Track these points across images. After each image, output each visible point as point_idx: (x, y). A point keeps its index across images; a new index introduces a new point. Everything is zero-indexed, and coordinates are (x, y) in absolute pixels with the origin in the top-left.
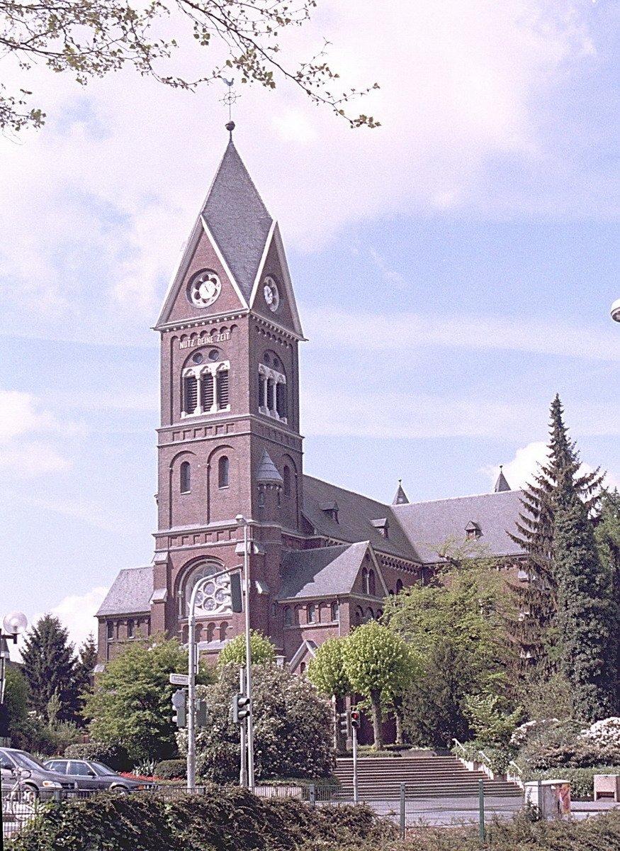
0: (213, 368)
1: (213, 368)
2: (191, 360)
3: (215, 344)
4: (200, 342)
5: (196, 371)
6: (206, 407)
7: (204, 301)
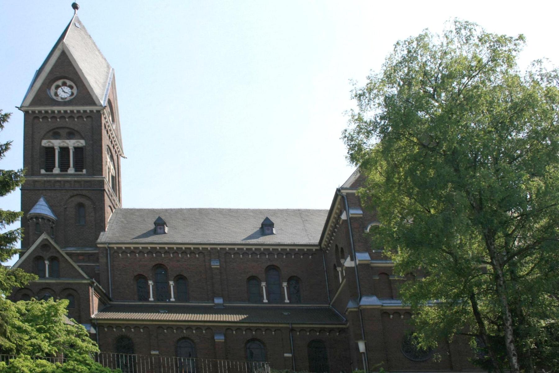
1: (71, 144)
5: (57, 143)
6: (64, 166)
7: (56, 94)
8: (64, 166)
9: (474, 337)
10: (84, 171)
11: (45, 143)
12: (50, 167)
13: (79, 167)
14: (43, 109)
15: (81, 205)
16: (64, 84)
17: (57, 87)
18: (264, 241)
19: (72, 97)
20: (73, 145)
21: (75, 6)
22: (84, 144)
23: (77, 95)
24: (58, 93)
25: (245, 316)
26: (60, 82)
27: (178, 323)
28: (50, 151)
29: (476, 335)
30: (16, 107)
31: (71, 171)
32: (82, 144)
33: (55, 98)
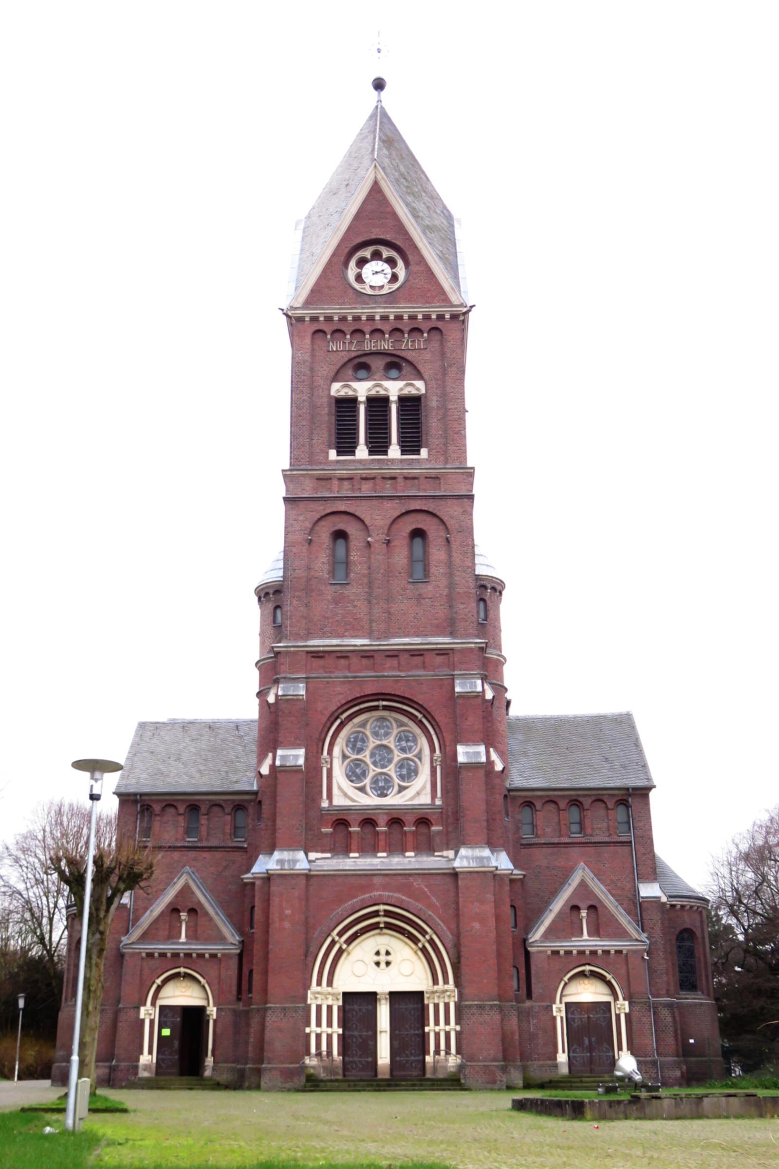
0: (394, 389)
1: (394, 389)
2: (351, 365)
3: (395, 352)
4: (370, 345)
5: (362, 389)
6: (378, 445)
7: (359, 278)
8: (378, 445)
9: (772, 945)
10: (424, 453)
11: (337, 389)
12: (346, 445)
13: (410, 444)
14: (335, 311)
15: (418, 534)
16: (377, 256)
17: (362, 262)
18: (433, 432)
19: (396, 286)
20: (397, 394)
21: (379, 85)
22: (423, 391)
23: (406, 281)
24: (364, 276)
25: (68, 874)
26: (367, 253)
27: (551, 793)
28: (347, 405)
29: (156, 815)
30: (280, 309)
31: (394, 451)
32: (418, 389)
33: (357, 286)
